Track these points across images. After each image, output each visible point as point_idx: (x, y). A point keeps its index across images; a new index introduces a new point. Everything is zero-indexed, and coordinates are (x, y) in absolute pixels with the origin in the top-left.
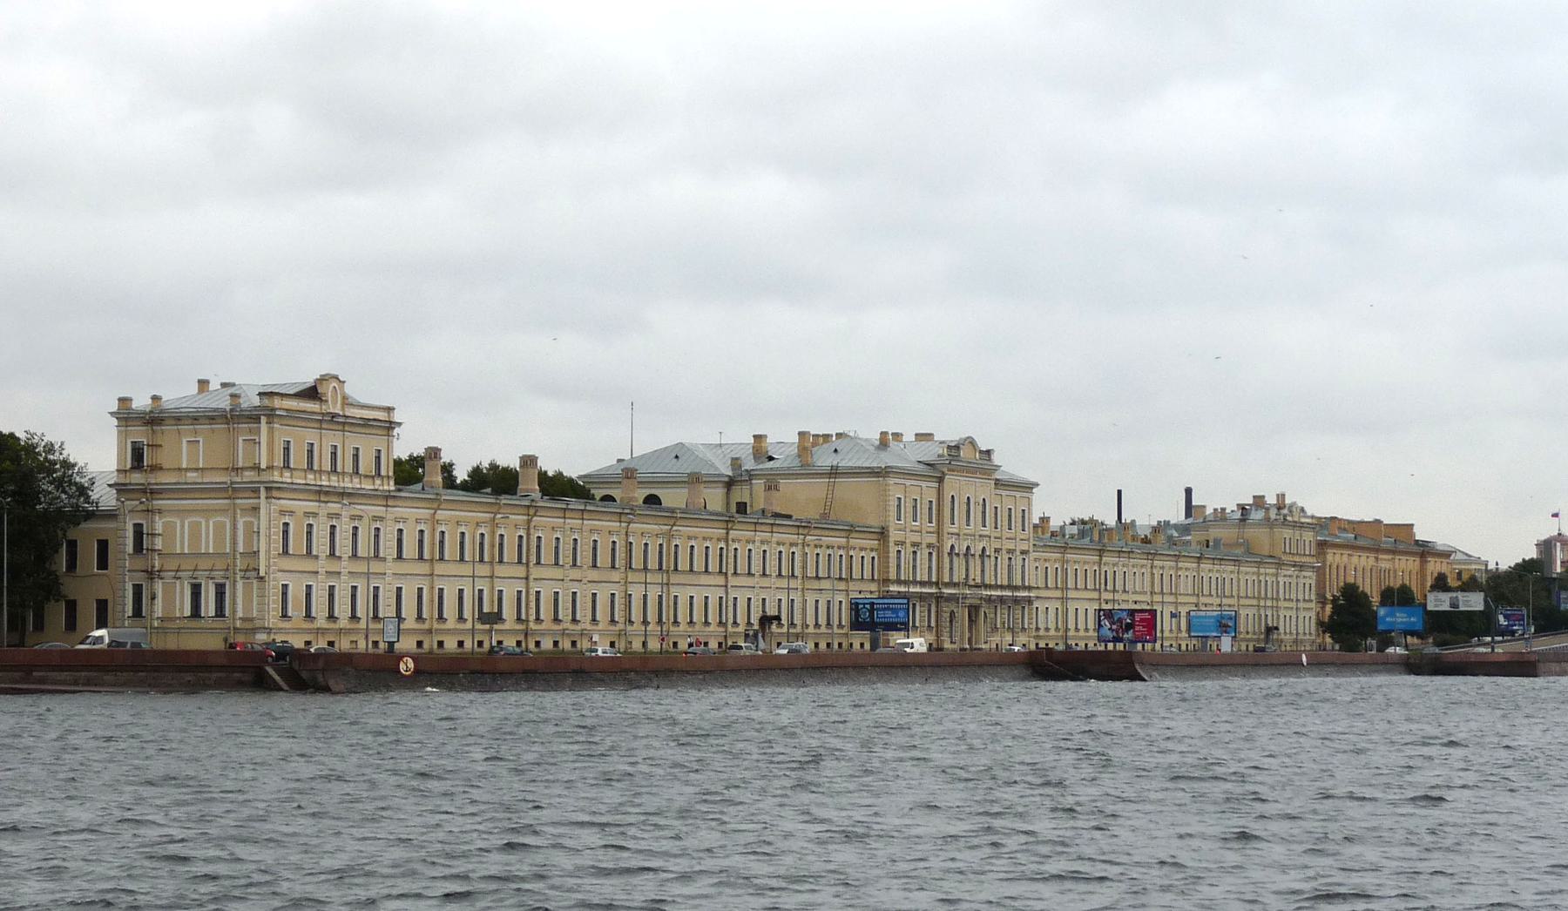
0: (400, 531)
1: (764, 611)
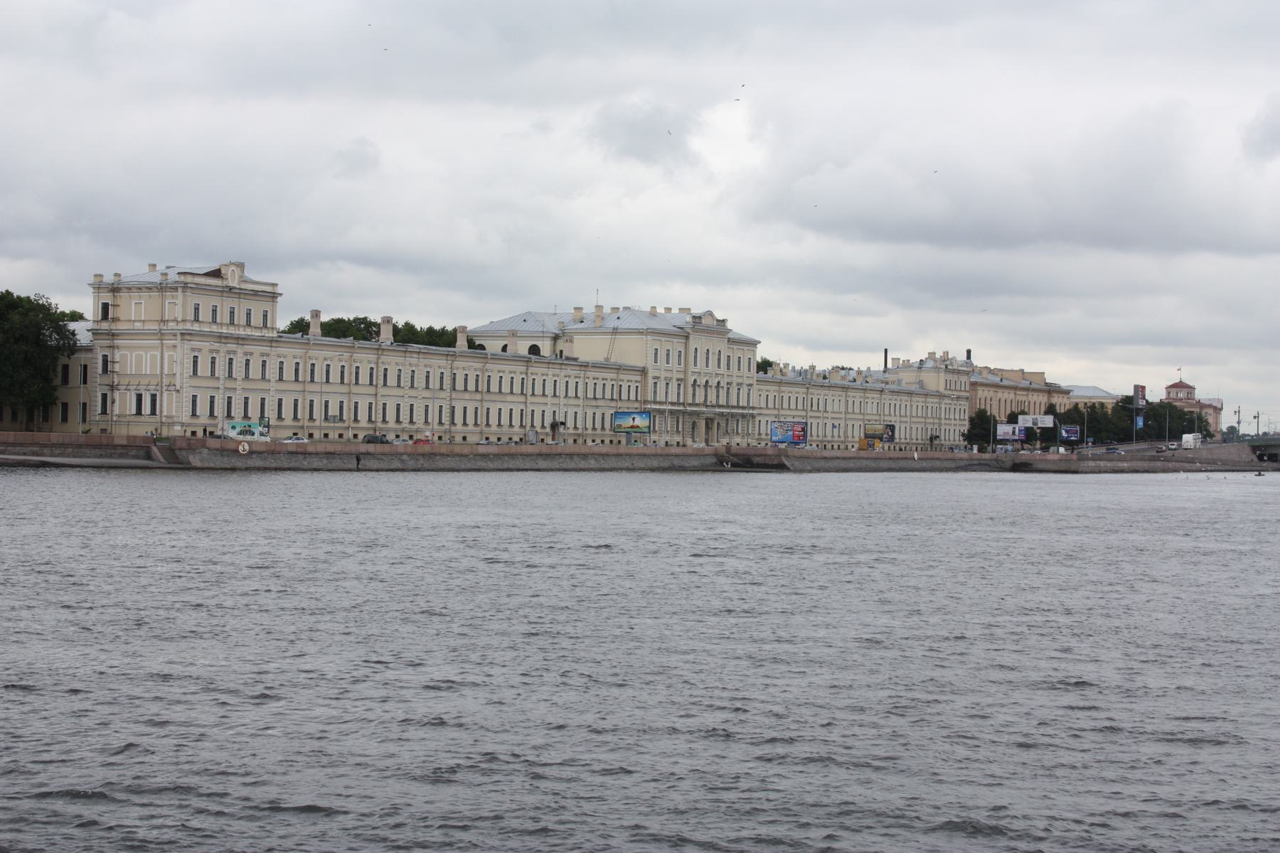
0: (512, 378)
1: (554, 419)
